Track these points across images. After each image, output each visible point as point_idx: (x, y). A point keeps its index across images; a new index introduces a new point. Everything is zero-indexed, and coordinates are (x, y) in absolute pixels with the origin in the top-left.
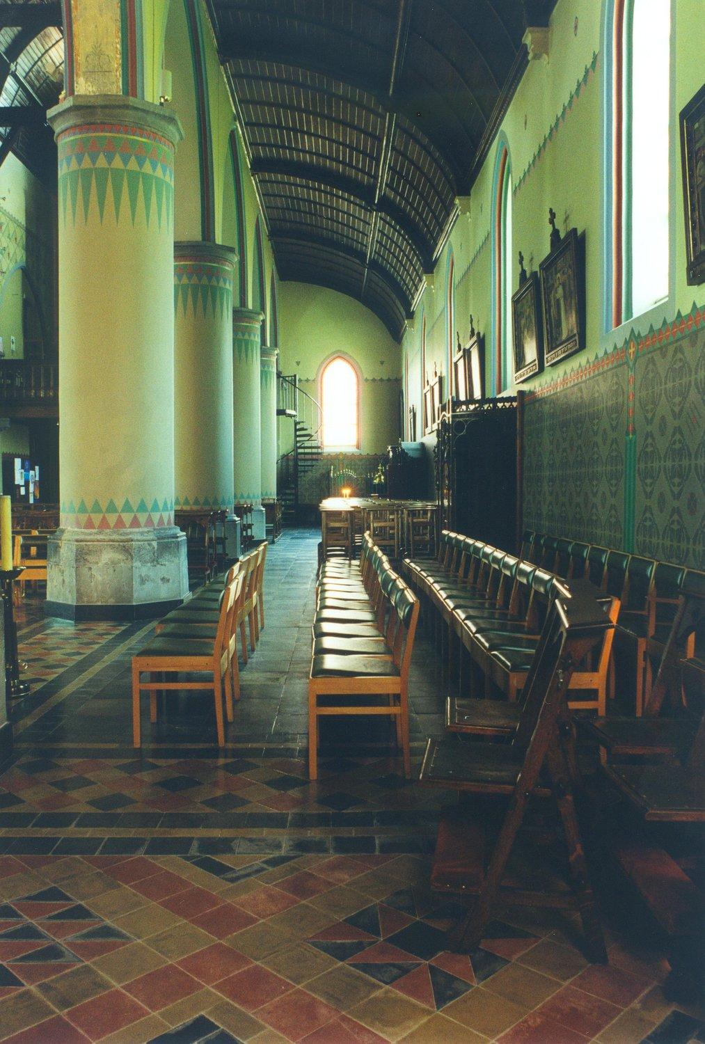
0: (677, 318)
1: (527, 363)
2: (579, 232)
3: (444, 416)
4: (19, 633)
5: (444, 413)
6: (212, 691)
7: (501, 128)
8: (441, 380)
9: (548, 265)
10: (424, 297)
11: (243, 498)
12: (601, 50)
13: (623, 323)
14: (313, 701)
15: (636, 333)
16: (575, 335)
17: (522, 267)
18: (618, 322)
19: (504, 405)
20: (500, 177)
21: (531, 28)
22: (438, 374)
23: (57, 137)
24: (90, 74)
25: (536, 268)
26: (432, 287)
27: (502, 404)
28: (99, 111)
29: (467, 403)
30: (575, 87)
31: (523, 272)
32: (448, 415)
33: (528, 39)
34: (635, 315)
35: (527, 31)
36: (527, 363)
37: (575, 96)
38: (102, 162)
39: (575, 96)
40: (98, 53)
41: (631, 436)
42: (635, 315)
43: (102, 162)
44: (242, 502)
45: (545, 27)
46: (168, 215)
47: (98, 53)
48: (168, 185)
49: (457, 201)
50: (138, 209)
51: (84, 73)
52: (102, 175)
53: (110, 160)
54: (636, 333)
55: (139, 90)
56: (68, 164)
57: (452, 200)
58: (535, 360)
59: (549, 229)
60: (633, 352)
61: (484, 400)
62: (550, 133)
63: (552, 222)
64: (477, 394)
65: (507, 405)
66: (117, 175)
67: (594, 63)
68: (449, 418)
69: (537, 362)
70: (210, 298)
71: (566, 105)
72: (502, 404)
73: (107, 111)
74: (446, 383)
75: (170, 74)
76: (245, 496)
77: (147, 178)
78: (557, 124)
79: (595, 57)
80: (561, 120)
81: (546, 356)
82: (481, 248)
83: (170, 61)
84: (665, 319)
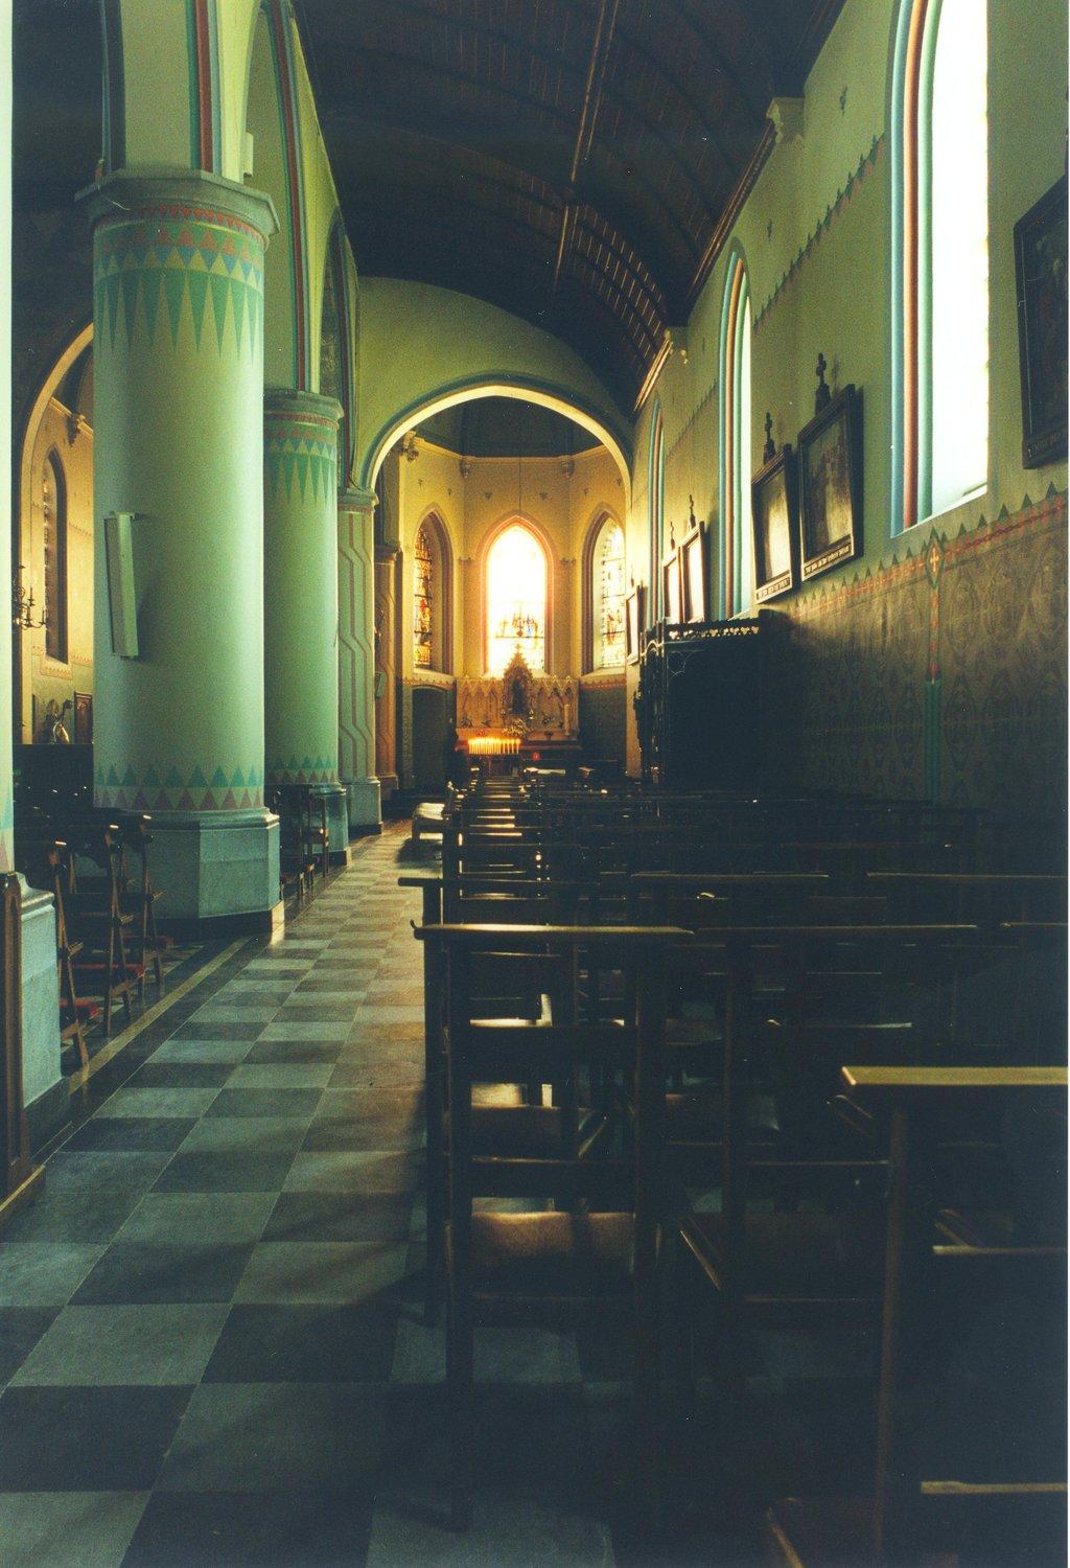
0: (960, 534)
1: (775, 574)
2: (857, 388)
3: (653, 645)
4: (23, 905)
5: (653, 642)
7: (734, 233)
8: (641, 592)
9: (809, 436)
10: (661, 389)
12: (886, 137)
13: (920, 522)
15: (940, 536)
16: (848, 536)
17: (769, 436)
18: (913, 520)
19: (740, 631)
21: (778, 99)
22: (637, 583)
25: (794, 442)
26: (684, 353)
27: (737, 630)
29: (681, 628)
30: (857, 166)
31: (770, 445)
32: (658, 645)
33: (775, 113)
34: (937, 510)
35: (773, 102)
36: (775, 574)
37: (824, 227)
39: (815, 242)
41: (933, 682)
42: (937, 510)
45: (799, 97)
46: (252, 333)
48: (252, 293)
49: (667, 334)
54: (940, 536)
55: (307, 385)
56: (106, 267)
57: (661, 332)
58: (787, 572)
59: (816, 382)
60: (937, 563)
61: (709, 622)
62: (837, 203)
63: (820, 372)
64: (698, 614)
65: (745, 630)
67: (873, 152)
68: (660, 649)
69: (790, 575)
71: (853, 175)
72: (737, 630)
74: (649, 597)
75: (250, 138)
77: (315, 460)
78: (818, 235)
79: (876, 144)
80: (815, 242)
81: (803, 566)
82: (704, 403)
83: (252, 123)
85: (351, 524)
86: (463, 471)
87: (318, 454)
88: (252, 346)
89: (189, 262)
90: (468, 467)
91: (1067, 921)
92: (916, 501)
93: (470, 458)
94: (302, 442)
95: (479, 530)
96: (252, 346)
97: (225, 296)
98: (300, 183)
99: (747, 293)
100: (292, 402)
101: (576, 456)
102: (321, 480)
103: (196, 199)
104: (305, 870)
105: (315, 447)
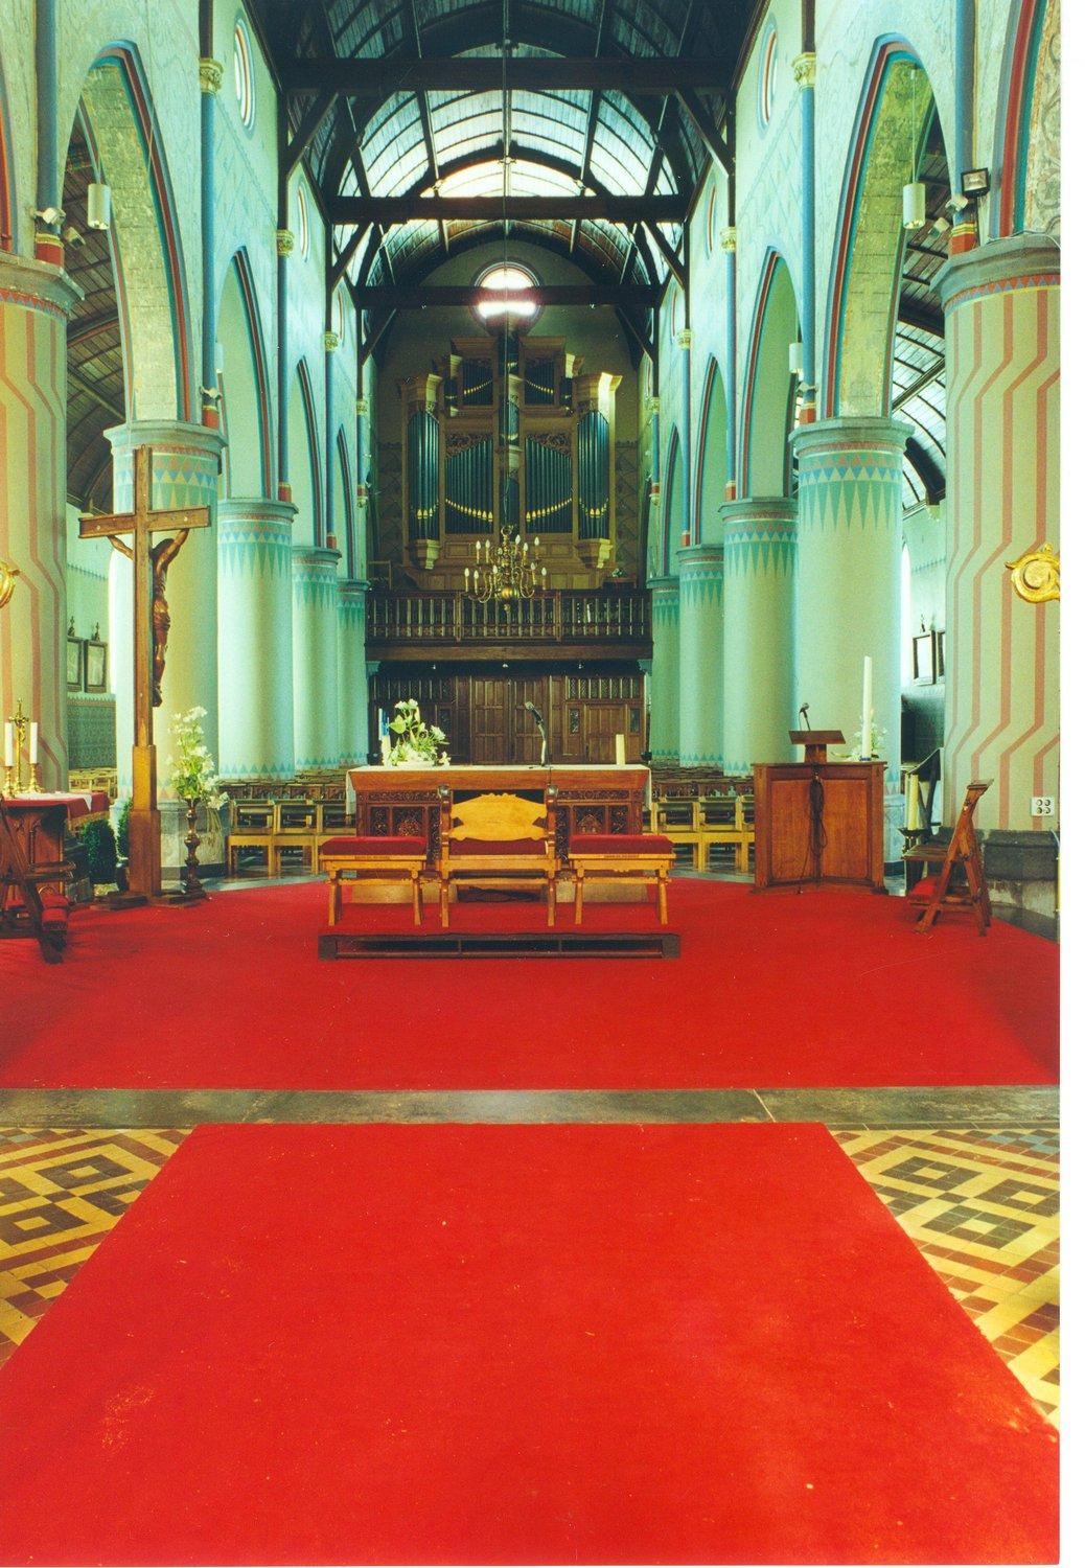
6: (614, 763)
11: (276, 770)
14: (117, 36)
20: (738, 326)
23: (955, 756)
24: (854, 398)
28: (863, 431)
38: (849, 475)
40: (861, 380)
43: (849, 475)
44: (323, 768)
47: (861, 380)
50: (867, 515)
51: (849, 398)
52: (849, 486)
53: (856, 472)
66: (863, 486)
70: (882, 496)
73: (869, 431)
76: (286, 767)
84: (980, 1173)
102: (276, 560)
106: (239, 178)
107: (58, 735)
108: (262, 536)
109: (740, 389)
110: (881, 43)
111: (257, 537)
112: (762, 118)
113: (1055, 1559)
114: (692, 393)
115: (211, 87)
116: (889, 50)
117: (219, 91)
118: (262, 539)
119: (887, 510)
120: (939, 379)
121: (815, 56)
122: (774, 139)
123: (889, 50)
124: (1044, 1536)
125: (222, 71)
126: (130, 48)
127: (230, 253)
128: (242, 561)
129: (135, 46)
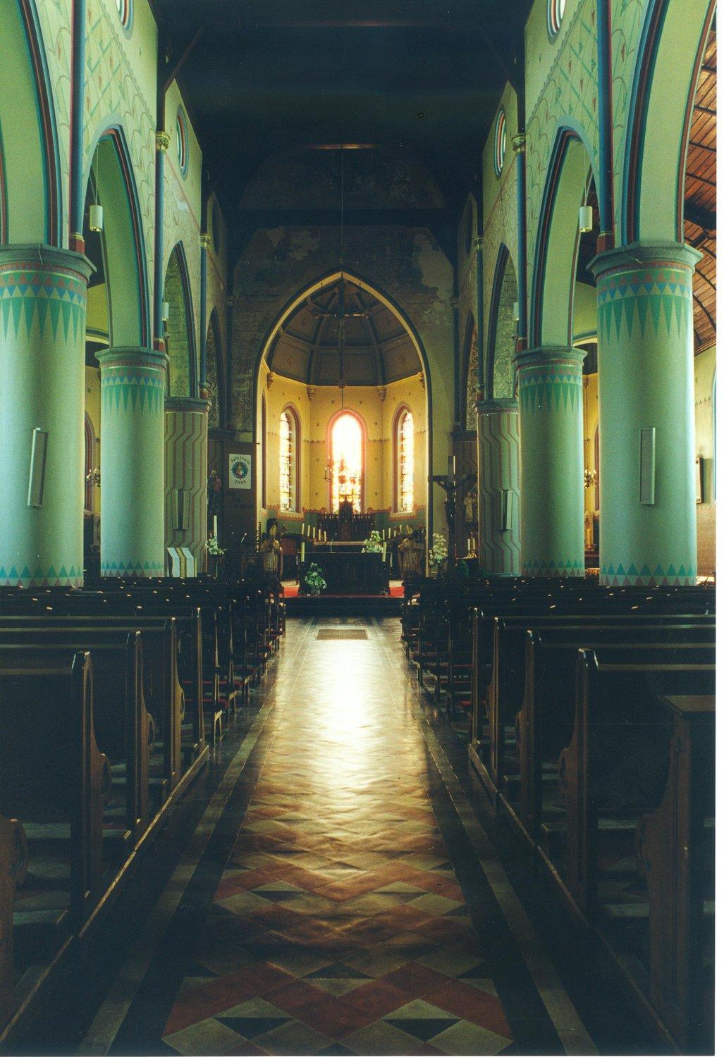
77: (577, 385)
85: (193, 420)
86: (309, 394)
87: (152, 385)
88: (75, 333)
89: (651, 290)
90: (313, 391)
91: (714, 663)
92: (417, 419)
93: (313, 386)
94: (150, 380)
95: (322, 422)
96: (75, 333)
97: (659, 304)
98: (625, 217)
99: (505, 131)
100: (568, 354)
101: (589, 376)
102: (146, 400)
103: (678, 258)
104: (328, 518)
105: (572, 378)
106: (105, 83)
107: (518, 487)
108: (134, 380)
109: (531, 259)
110: (563, 130)
111: (130, 380)
112: (548, 32)
113: (714, 1055)
114: (529, 193)
115: (163, 148)
116: (567, 134)
117: (167, 151)
118: (134, 381)
119: (572, 403)
120: (705, 246)
121: (525, 136)
122: (542, 91)
123: (567, 134)
124: (708, 1045)
125: (169, 137)
126: (118, 128)
127: (172, 245)
128: (118, 400)
129: (121, 127)
